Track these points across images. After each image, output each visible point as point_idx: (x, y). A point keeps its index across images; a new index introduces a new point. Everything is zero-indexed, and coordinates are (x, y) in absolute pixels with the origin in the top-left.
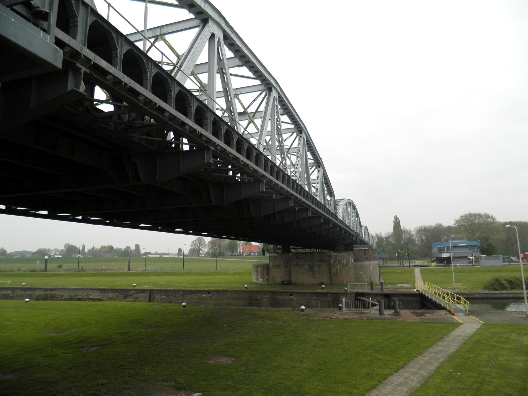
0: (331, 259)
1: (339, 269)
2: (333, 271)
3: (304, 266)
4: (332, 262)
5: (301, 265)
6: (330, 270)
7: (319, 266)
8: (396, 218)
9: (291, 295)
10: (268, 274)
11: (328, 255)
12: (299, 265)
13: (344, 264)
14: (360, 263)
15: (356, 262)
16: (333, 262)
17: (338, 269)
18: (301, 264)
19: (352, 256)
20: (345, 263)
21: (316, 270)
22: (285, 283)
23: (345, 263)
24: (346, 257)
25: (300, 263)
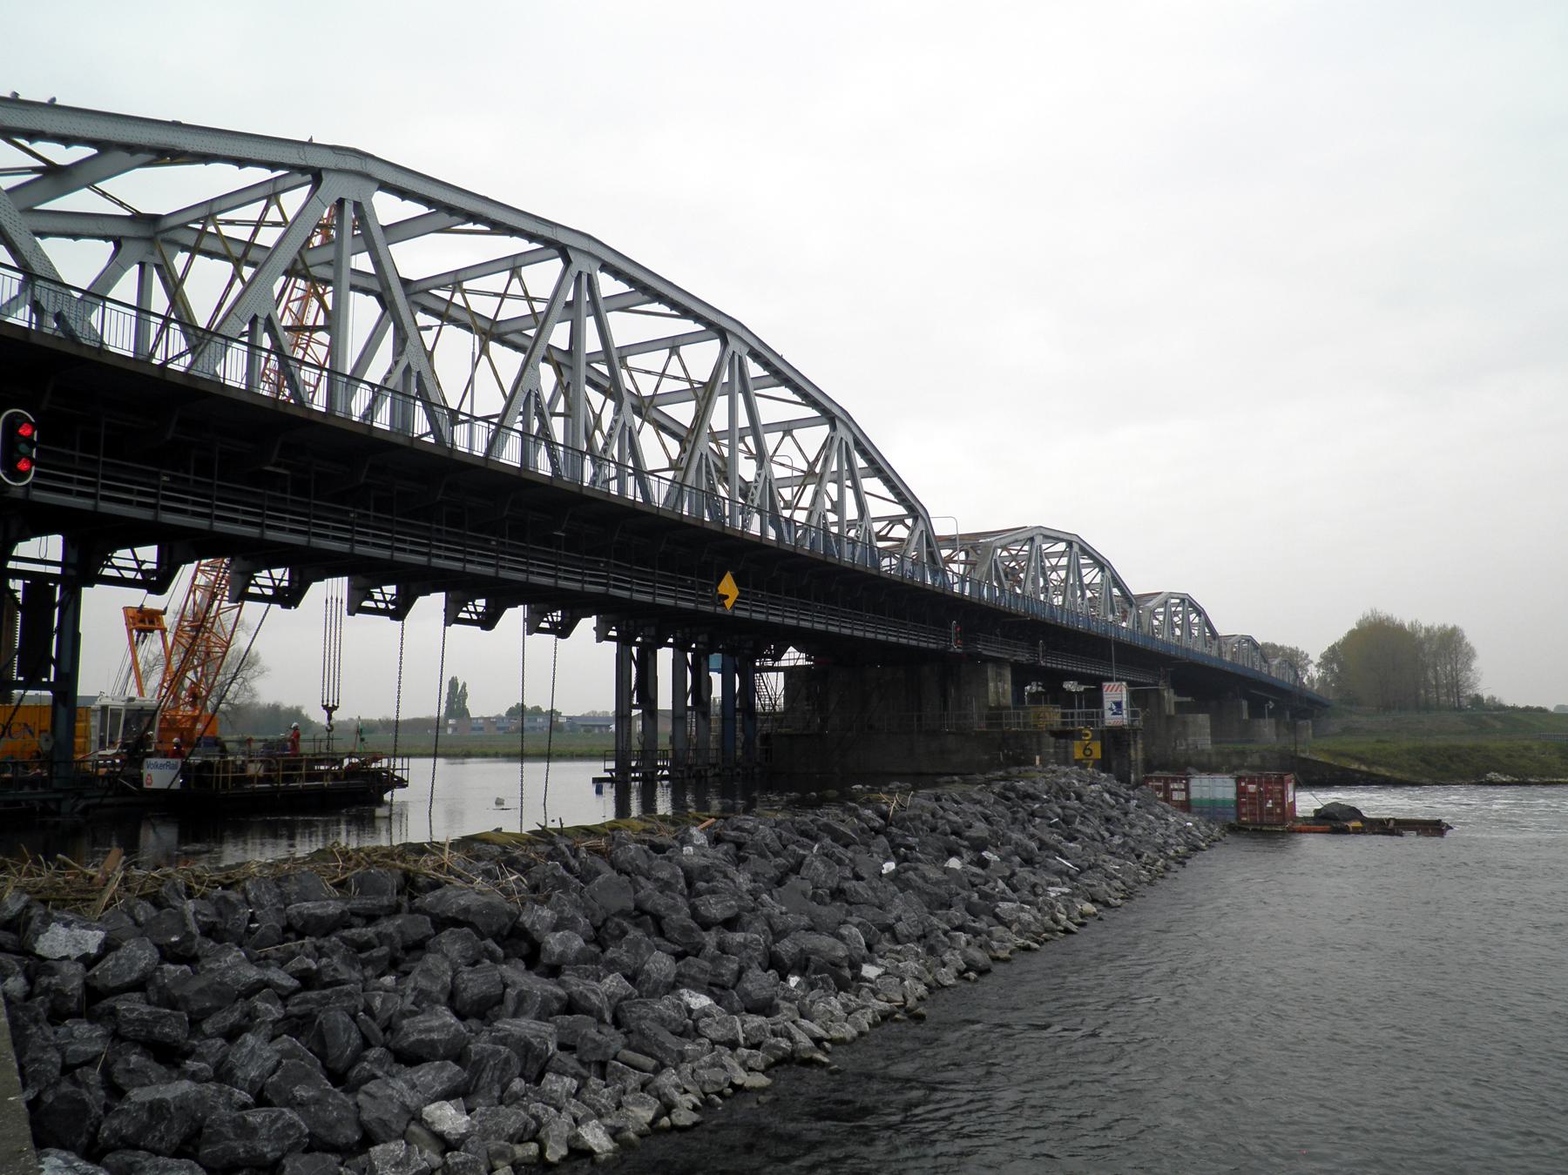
8: (453, 683)
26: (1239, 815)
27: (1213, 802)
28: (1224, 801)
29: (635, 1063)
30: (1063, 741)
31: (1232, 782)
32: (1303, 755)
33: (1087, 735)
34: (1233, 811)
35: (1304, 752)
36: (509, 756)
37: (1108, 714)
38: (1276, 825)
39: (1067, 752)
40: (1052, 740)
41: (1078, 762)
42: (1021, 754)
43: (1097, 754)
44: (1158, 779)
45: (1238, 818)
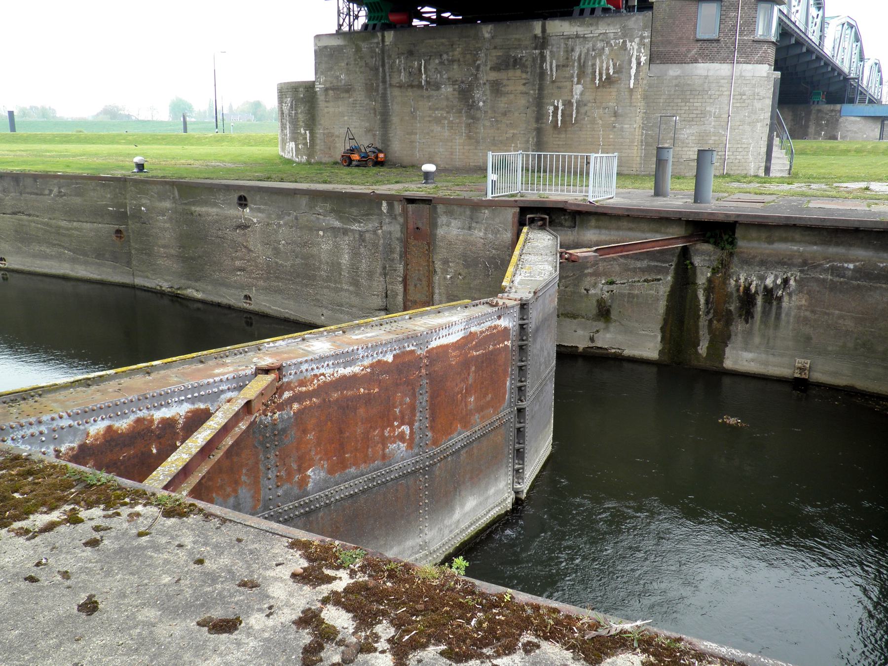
0: (547, 53)
1: (578, 102)
2: (551, 109)
3: (437, 87)
4: (550, 65)
5: (428, 83)
6: (539, 103)
7: (497, 88)
9: (243, 202)
10: (312, 122)
11: (536, 36)
12: (420, 86)
13: (601, 74)
14: (674, 71)
15: (657, 68)
16: (557, 66)
17: (574, 101)
18: (426, 81)
19: (642, 38)
20: (608, 74)
21: (481, 104)
22: (356, 157)
23: (608, 74)
24: (612, 42)
25: (424, 76)
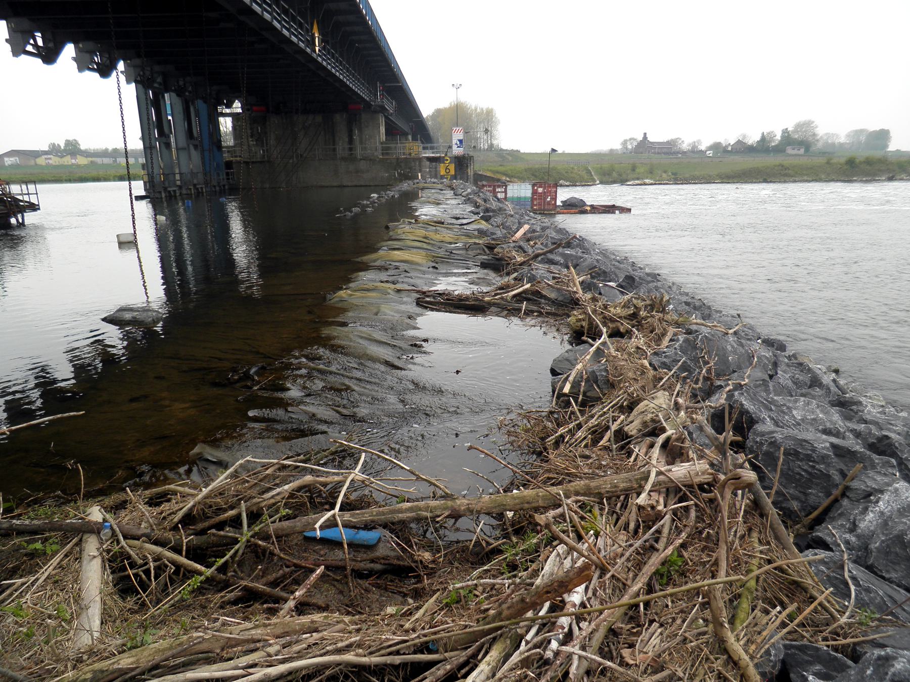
8: (104, 320)
26: (533, 205)
27: (519, 198)
28: (525, 198)
29: (386, 347)
30: (434, 164)
31: (530, 187)
32: (480, 173)
33: (447, 160)
34: (529, 203)
35: (480, 171)
36: (121, 179)
37: (455, 147)
38: (551, 210)
39: (436, 171)
40: (428, 163)
41: (442, 177)
42: (408, 172)
43: (452, 172)
44: (490, 186)
45: (532, 207)
